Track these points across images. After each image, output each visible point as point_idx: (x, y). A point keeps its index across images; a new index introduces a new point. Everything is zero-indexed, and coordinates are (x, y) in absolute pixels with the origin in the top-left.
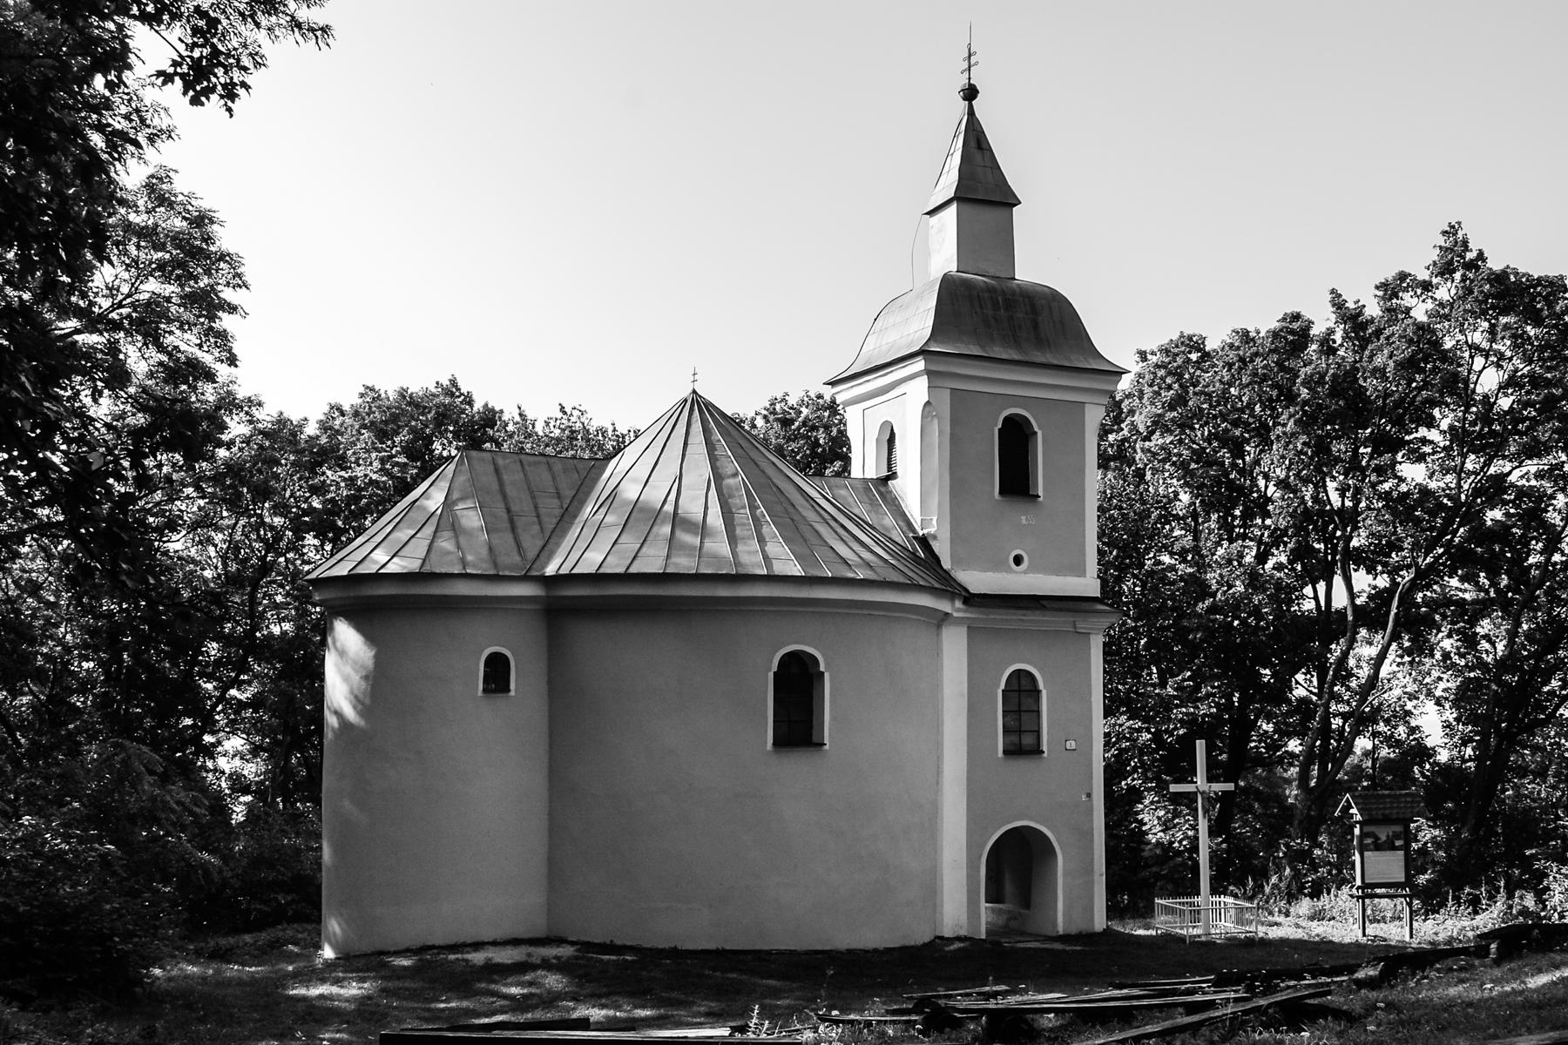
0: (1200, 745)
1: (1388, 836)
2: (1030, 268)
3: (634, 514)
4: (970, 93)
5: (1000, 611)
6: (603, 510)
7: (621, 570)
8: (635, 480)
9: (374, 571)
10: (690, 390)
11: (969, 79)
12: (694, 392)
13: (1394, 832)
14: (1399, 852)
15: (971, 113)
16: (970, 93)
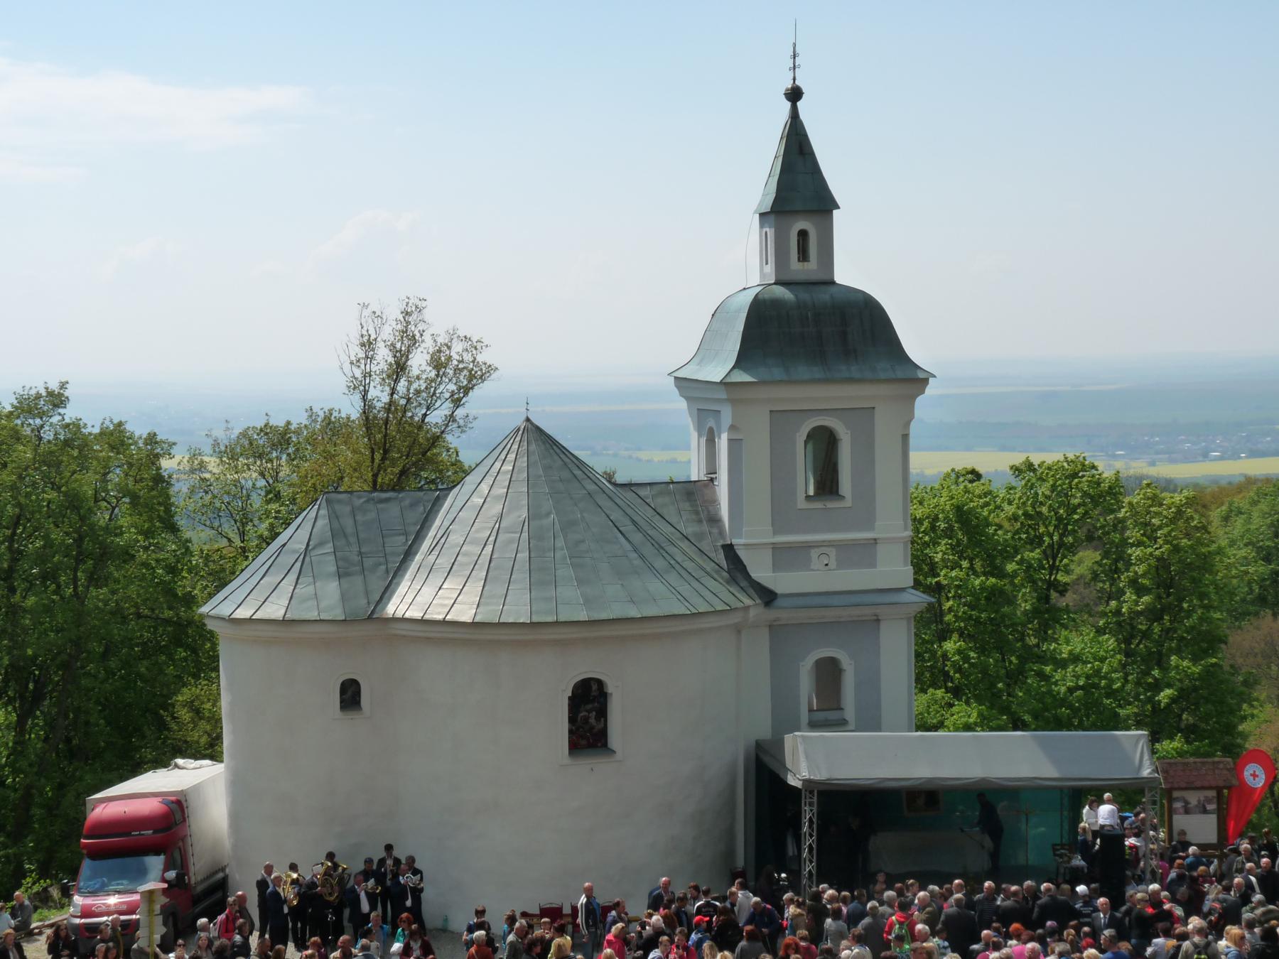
0: (1058, 852)
1: (1199, 801)
2: (848, 272)
3: (454, 567)
4: (794, 95)
5: (773, 249)
6: (436, 552)
7: (440, 617)
8: (491, 476)
9: (248, 617)
10: (524, 418)
11: (794, 79)
12: (528, 420)
13: (1206, 797)
14: (1211, 815)
15: (795, 115)
16: (794, 95)
